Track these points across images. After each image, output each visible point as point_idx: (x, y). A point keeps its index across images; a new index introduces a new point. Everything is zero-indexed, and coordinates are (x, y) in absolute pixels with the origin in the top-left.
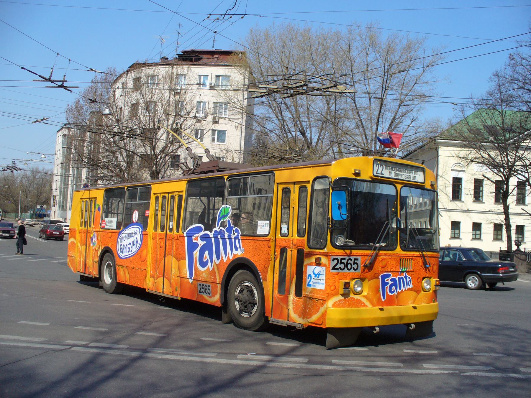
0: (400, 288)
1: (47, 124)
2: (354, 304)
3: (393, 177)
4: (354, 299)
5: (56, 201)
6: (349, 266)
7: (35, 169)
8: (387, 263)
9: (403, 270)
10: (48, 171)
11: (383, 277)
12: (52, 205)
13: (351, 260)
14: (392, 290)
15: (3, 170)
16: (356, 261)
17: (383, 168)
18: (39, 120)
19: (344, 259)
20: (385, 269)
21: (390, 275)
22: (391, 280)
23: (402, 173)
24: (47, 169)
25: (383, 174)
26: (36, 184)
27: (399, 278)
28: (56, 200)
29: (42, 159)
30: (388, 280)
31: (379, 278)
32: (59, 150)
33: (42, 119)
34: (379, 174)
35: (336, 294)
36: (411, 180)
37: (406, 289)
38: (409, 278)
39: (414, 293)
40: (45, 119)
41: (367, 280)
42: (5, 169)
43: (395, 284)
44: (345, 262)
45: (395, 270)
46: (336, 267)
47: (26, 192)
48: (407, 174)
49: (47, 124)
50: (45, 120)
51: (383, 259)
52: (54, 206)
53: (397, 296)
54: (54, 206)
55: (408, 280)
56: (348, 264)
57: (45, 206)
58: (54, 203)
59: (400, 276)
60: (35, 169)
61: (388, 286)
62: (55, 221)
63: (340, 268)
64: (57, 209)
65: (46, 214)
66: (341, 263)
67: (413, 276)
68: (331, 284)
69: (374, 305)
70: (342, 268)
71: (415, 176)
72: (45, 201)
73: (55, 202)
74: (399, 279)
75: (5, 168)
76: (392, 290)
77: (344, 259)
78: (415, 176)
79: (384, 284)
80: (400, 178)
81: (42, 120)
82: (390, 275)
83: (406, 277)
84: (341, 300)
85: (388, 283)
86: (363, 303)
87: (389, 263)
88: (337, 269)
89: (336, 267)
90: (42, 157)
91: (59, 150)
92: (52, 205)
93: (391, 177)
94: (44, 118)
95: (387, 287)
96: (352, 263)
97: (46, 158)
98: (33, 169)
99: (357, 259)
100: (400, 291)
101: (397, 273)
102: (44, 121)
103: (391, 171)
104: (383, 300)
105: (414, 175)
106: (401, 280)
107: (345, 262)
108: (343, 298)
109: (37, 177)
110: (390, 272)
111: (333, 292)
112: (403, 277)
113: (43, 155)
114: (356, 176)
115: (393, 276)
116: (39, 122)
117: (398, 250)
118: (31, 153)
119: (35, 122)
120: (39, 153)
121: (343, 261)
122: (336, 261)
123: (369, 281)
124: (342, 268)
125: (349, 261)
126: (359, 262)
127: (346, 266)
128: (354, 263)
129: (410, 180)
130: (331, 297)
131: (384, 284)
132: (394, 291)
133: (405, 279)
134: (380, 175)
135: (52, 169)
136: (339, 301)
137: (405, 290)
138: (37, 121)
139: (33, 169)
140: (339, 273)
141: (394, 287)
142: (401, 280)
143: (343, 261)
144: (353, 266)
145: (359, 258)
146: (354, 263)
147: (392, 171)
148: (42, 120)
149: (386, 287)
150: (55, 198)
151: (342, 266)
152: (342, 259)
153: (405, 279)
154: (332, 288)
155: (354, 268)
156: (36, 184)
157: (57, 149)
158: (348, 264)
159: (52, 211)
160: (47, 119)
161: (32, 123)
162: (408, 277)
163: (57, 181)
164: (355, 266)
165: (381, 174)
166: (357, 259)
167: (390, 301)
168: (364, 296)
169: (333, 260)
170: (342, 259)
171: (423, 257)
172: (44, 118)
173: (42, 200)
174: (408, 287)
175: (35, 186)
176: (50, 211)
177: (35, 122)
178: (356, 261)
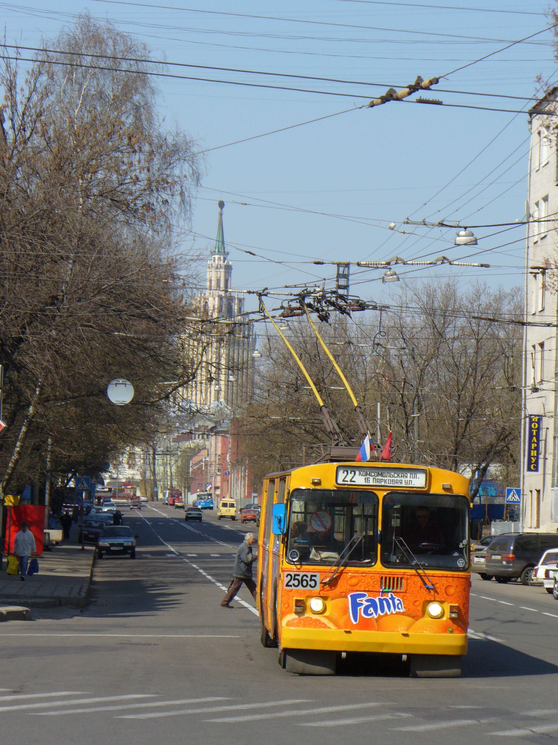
0: (382, 610)
1: (439, 103)
2: (311, 624)
3: (371, 483)
4: (311, 619)
5: (542, 444)
6: (305, 583)
7: (439, 294)
8: (360, 581)
9: (387, 590)
10: (499, 299)
11: (354, 598)
12: (524, 461)
13: (307, 576)
14: (369, 612)
15: (283, 315)
16: (313, 578)
17: (355, 474)
18: (400, 92)
19: (299, 575)
20: (357, 588)
21: (365, 595)
22: (367, 601)
23: (388, 478)
24: (493, 290)
25: (354, 482)
26: (446, 364)
27: (379, 599)
28: (542, 437)
29: (444, 254)
30: (361, 601)
31: (347, 598)
32: (546, 199)
33: (410, 87)
34: (347, 481)
35: (290, 612)
36: (403, 485)
37: (394, 612)
38: (398, 600)
39: (409, 619)
40: (425, 83)
41: (329, 599)
42: (292, 309)
43: (373, 604)
44: (300, 578)
45: (371, 589)
46: (289, 584)
47: (404, 405)
48: (395, 479)
49: (439, 103)
50: (427, 88)
51: (351, 577)
52: (533, 466)
53: (377, 620)
54: (533, 466)
55: (397, 602)
56: (302, 580)
57: (494, 469)
58: (534, 453)
59: (382, 596)
60: (439, 294)
61: (363, 607)
62: (537, 536)
63: (294, 585)
64: (549, 479)
65: (501, 506)
66: (295, 579)
67: (405, 598)
68: (285, 602)
69: (339, 627)
70: (296, 584)
71: (411, 479)
72: (492, 446)
73: (537, 449)
74: (381, 601)
75: (295, 305)
76: (369, 612)
77: (299, 575)
78: (411, 479)
79: (355, 605)
80: (383, 484)
81: (413, 89)
82: (365, 595)
83: (392, 599)
84: (295, 619)
85: (362, 604)
86: (324, 624)
87: (363, 581)
88: (291, 586)
89: (289, 584)
90: (460, 240)
91: (546, 199)
92: (524, 461)
93: (367, 484)
94: (420, 79)
95: (360, 609)
96: (308, 579)
97: (475, 242)
98: (431, 296)
99: (315, 576)
100: (381, 614)
101: (378, 594)
102: (421, 94)
103: (368, 476)
104: (354, 623)
105: (408, 479)
106: (384, 602)
107: (300, 578)
108: (297, 617)
109: (450, 333)
110: (365, 591)
111: (287, 610)
112: (388, 598)
113: (462, 233)
114: (315, 486)
115: (369, 596)
116: (398, 99)
117: (378, 567)
118: (408, 228)
119: (385, 100)
120: (442, 224)
121: (297, 577)
122: (289, 577)
123: (332, 600)
124: (296, 584)
125: (305, 578)
126: (318, 579)
127: (301, 582)
128: (311, 580)
129: (401, 485)
130: (285, 616)
131: (355, 605)
132: (372, 614)
133: (390, 601)
134: (349, 483)
135: (519, 289)
136: (293, 620)
137: (392, 613)
138: (390, 97)
139: (429, 296)
140: (292, 590)
141: (371, 609)
142: (384, 602)
143: (297, 577)
144: (310, 583)
145: (318, 574)
146: (311, 580)
147: (370, 477)
148: (413, 89)
149: (359, 608)
150: (538, 429)
151: (296, 583)
152: (295, 575)
153: (390, 601)
154: (286, 606)
155: (310, 586)
156: (446, 364)
157: (536, 195)
158: (302, 580)
159: (527, 492)
160: (431, 83)
161: (372, 105)
162: (397, 598)
163: (542, 345)
164: (313, 583)
165: (351, 481)
166: (315, 576)
167: (365, 625)
168: (325, 616)
169: (287, 576)
170: (295, 575)
171: (419, 575)
172: (420, 79)
173: (479, 441)
174: (397, 610)
175: (443, 372)
176: (518, 492)
177: (385, 100)
178: (313, 578)
